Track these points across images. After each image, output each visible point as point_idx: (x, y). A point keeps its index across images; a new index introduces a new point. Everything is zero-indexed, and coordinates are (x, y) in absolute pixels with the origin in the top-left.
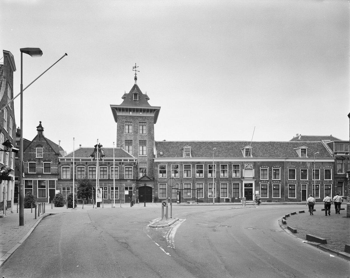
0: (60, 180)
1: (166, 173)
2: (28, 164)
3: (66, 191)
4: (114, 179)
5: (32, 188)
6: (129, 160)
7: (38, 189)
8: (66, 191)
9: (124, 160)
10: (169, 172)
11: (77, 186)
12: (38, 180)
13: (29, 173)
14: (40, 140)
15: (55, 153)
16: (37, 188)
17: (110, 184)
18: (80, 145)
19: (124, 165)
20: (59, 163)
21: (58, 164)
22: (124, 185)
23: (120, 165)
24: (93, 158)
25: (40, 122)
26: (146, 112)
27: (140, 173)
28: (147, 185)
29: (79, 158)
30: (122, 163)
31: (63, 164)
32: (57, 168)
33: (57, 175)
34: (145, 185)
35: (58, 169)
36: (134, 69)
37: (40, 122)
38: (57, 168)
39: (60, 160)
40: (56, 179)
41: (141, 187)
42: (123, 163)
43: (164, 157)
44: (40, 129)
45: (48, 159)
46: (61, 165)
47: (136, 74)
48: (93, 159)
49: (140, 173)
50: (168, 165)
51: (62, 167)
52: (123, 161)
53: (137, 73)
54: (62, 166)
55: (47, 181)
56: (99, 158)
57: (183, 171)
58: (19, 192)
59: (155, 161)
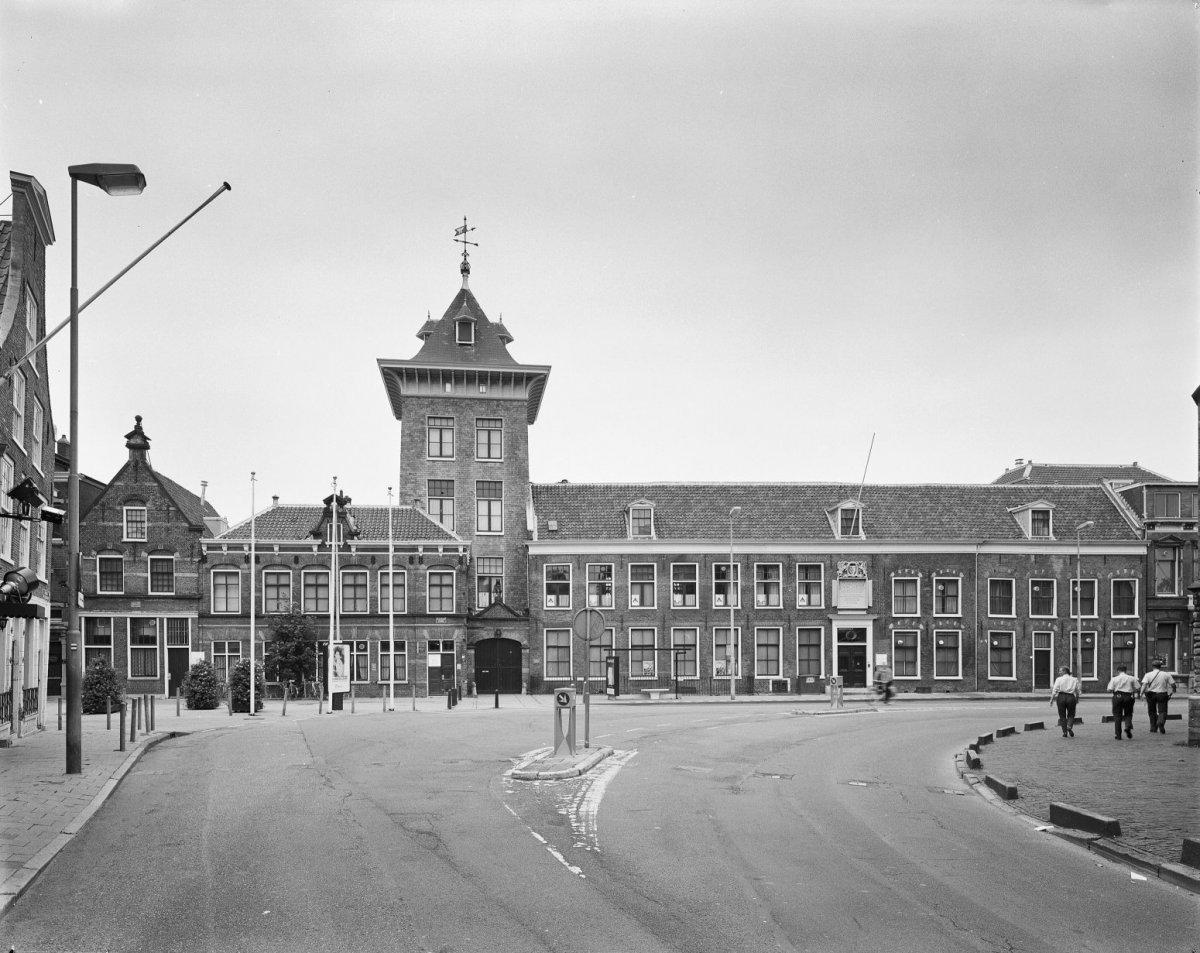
0: (204, 616)
1: (568, 593)
2: (95, 561)
3: (227, 654)
4: (391, 614)
5: (110, 644)
6: (441, 550)
7: (129, 647)
8: (227, 654)
9: (426, 549)
10: (580, 588)
11: (263, 638)
12: (131, 618)
13: (99, 592)
14: (136, 481)
15: (190, 523)
16: (126, 646)
17: (376, 632)
18: (275, 498)
19: (424, 566)
20: (204, 559)
21: (199, 561)
22: (425, 633)
23: (411, 567)
24: (319, 542)
25: (139, 419)
26: (501, 384)
27: (480, 594)
28: (505, 635)
29: (272, 541)
30: (417, 560)
31: (217, 562)
32: (196, 575)
33: (196, 598)
34: (496, 634)
35: (198, 580)
36: (461, 237)
37: (139, 419)
38: (196, 575)
39: (204, 548)
40: (192, 615)
41: (484, 641)
42: (421, 560)
43: (564, 537)
44: (138, 441)
45: (165, 546)
46: (208, 565)
47: (465, 254)
48: (319, 546)
49: (480, 594)
50: (576, 565)
51: (212, 571)
52: (421, 552)
53: (470, 249)
54: (213, 567)
55: (161, 620)
56: (339, 541)
57: (627, 587)
58: (64, 657)
59: (532, 551)
